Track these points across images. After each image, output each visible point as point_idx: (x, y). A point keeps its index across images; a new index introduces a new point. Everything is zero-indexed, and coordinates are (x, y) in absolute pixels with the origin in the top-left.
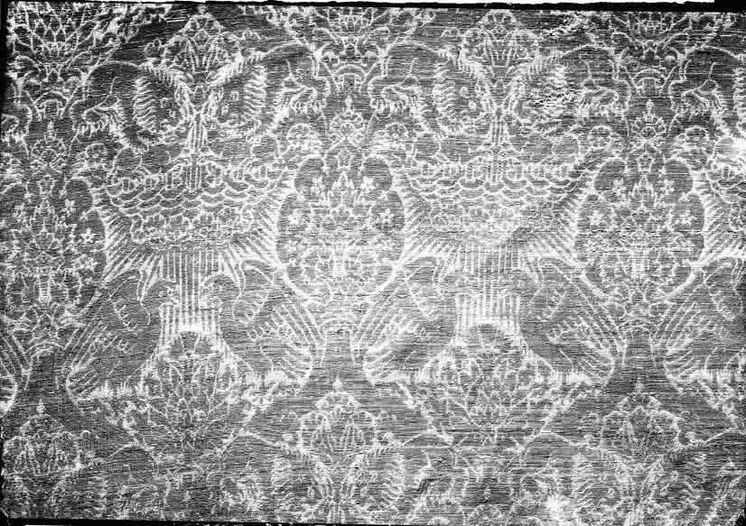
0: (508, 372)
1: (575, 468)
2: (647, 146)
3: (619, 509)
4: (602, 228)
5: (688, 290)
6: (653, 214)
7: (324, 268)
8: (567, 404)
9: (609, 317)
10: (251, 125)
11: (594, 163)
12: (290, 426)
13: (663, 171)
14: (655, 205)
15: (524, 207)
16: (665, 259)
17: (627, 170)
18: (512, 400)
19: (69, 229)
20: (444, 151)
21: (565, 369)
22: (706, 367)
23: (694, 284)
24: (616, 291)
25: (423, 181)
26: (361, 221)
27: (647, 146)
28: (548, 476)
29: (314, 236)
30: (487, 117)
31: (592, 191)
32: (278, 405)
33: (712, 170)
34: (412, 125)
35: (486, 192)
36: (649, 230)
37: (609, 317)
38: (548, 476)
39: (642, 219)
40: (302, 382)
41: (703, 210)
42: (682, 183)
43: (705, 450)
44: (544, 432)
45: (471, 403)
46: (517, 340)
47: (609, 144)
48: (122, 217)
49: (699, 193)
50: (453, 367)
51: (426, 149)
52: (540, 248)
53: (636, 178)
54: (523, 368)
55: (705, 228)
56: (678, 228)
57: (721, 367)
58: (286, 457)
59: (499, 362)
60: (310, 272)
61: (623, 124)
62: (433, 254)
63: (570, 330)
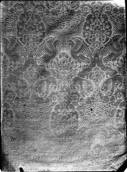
0: (68, 63)
1: (83, 84)
2: (97, 11)
3: (94, 92)
4: (89, 30)
5: (108, 43)
6: (100, 26)
7: (28, 39)
8: (81, 70)
9: (90, 50)
10: (75, 7)
11: (86, 15)
12: (21, 73)
13: (101, 16)
14: (100, 24)
15: (71, 26)
16: (103, 37)
17: (93, 16)
18: (69, 69)
19: (103, 25)
20: (119, 11)
21: (80, 62)
22: (111, 60)
23: (110, 41)
24: (92, 44)
25: (48, 20)
26: (36, 28)
27: (97, 11)
28: (78, 86)
29: (25, 31)
30: (60, 5)
31: (86, 21)
32: (19, 69)
33: (113, 15)
34: (44, 7)
35: (62, 22)
36: (99, 30)
37: (90, 50)
38: (78, 86)
39: (98, 27)
40: (23, 64)
41: (111, 25)
42: (106, 19)
43: (112, 78)
44: (77, 76)
45: (60, 70)
46: (70, 56)
47: (88, 10)
48: (116, 23)
49: (110, 21)
50: (56, 62)
51: (48, 12)
52: (75, 35)
53: (95, 18)
54: (71, 62)
55: (112, 29)
56: (106, 29)
57: (115, 60)
58: (21, 80)
59: (66, 60)
60: (25, 39)
61: (91, 6)
62: (52, 36)
63: (82, 53)
